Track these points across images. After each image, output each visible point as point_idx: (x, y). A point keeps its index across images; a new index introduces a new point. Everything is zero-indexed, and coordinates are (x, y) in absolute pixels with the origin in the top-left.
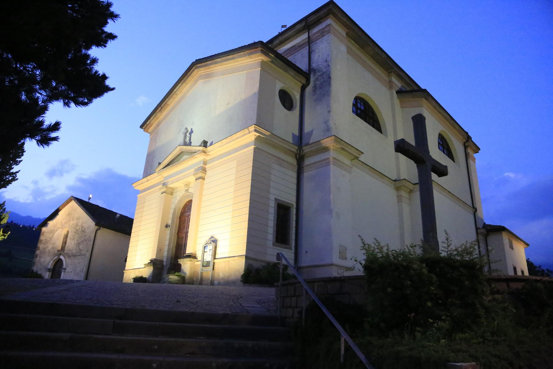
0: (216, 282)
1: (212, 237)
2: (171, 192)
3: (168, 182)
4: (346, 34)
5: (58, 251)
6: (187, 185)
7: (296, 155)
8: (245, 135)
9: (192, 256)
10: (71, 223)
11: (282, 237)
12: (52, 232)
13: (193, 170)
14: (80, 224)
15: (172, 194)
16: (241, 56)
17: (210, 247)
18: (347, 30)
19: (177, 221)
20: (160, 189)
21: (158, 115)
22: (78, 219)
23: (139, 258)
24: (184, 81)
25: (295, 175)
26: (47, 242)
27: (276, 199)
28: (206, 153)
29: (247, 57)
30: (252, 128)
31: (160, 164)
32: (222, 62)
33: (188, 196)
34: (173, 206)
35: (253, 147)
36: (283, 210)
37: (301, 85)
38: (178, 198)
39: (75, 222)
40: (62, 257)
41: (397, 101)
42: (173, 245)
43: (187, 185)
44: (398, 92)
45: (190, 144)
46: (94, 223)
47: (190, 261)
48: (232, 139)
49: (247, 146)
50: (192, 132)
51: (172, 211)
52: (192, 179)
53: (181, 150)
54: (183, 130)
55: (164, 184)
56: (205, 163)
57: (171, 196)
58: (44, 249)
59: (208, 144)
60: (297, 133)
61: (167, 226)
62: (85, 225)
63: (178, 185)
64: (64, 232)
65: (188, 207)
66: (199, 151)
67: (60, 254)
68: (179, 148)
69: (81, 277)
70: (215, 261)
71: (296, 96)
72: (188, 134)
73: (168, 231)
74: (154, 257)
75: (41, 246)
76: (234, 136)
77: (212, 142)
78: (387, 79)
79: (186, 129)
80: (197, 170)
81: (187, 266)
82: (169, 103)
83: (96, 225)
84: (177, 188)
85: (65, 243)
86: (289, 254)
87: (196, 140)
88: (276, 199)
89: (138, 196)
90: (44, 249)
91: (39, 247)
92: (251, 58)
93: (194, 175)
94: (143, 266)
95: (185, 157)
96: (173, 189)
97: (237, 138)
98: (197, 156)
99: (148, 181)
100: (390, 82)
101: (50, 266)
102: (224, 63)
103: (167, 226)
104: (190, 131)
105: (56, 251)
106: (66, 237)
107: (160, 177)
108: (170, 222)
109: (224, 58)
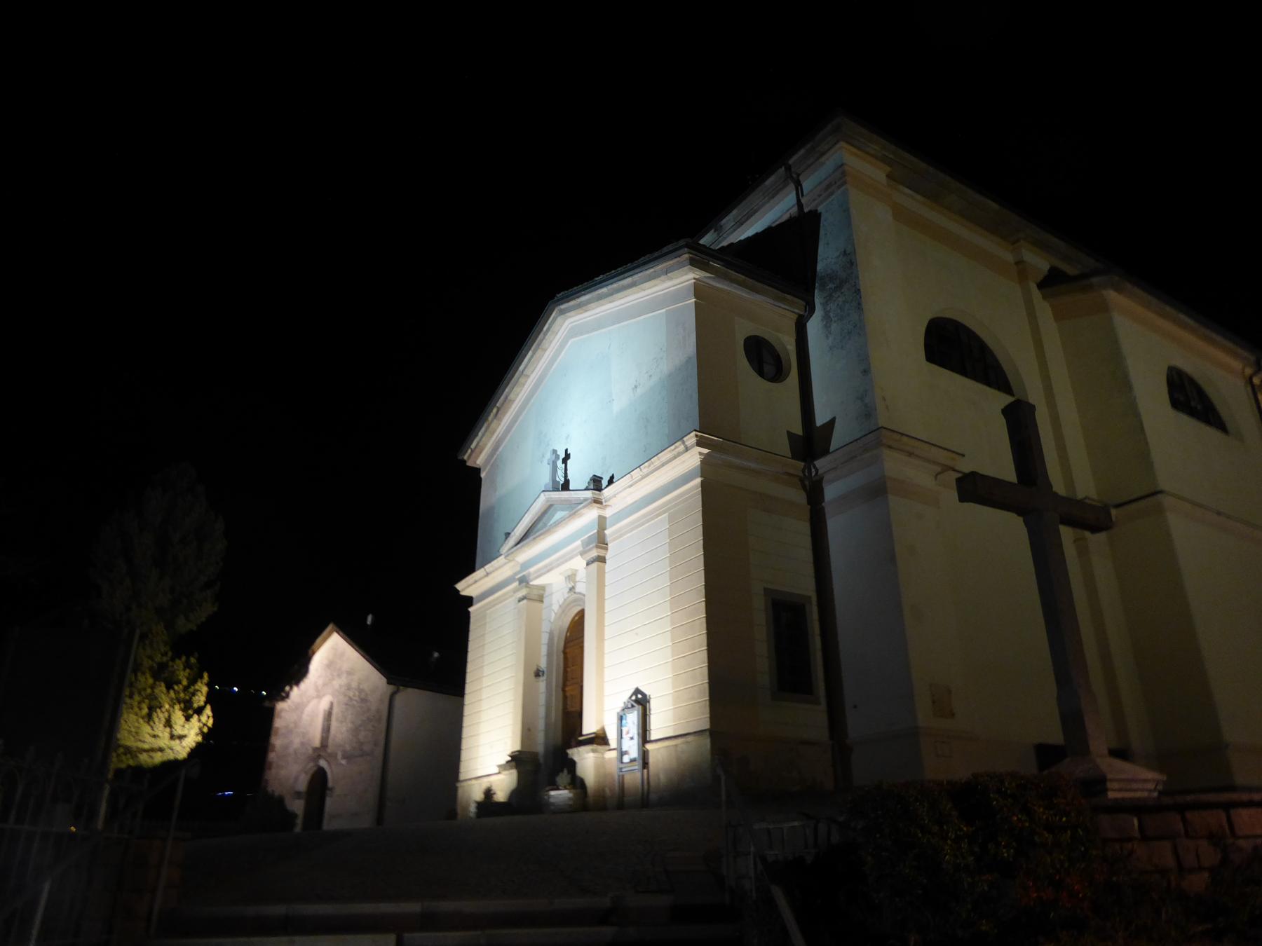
0: (653, 797)
1: (637, 691)
2: (538, 596)
3: (529, 574)
4: (888, 176)
5: (315, 749)
6: (571, 577)
7: (802, 481)
8: (679, 454)
9: (600, 739)
10: (337, 683)
11: (792, 676)
12: (299, 707)
13: (579, 543)
14: (354, 685)
15: (540, 599)
16: (650, 278)
17: (633, 718)
18: (888, 169)
19: (558, 659)
20: (515, 591)
21: (493, 425)
22: (349, 673)
23: (490, 750)
24: (539, 345)
25: (805, 527)
26: (290, 731)
27: (765, 589)
28: (601, 503)
29: (663, 277)
30: (691, 439)
31: (508, 535)
32: (611, 294)
33: (575, 601)
34: (546, 628)
35: (699, 480)
36: (787, 616)
37: (795, 317)
38: (556, 607)
39: (343, 680)
40: (323, 763)
41: (1044, 310)
42: (556, 715)
43: (571, 577)
44: (1041, 286)
45: (566, 486)
46: (384, 680)
47: (594, 751)
48: (652, 467)
49: (685, 479)
50: (567, 457)
51: (545, 639)
52: (579, 563)
53: (548, 501)
54: (549, 455)
55: (524, 581)
56: (602, 523)
57: (537, 604)
58: (286, 747)
59: (604, 483)
60: (798, 430)
61: (538, 674)
62: (365, 686)
63: (554, 581)
64: (324, 704)
65: (577, 625)
66: (586, 500)
67: (319, 757)
68: (543, 497)
69: (366, 822)
70: (649, 747)
71: (788, 343)
72: (560, 464)
73: (542, 684)
74: (517, 747)
75: (277, 742)
76: (656, 461)
77: (612, 477)
78: (1010, 258)
79: (555, 452)
80: (586, 544)
81: (587, 761)
82: (512, 396)
83: (389, 683)
84: (550, 585)
85: (327, 729)
86: (808, 720)
87: (579, 475)
88: (765, 589)
89: (471, 609)
90: (286, 747)
91: (274, 746)
92: (671, 279)
93: (582, 554)
94: (497, 770)
95: (559, 515)
96: (543, 588)
97: (663, 465)
98: (583, 511)
99: (488, 574)
100: (1019, 263)
101: (302, 785)
102: (619, 295)
103: (538, 674)
104: (563, 455)
105: (310, 751)
106: (329, 715)
107: (512, 564)
108: (543, 664)
109: (615, 285)
